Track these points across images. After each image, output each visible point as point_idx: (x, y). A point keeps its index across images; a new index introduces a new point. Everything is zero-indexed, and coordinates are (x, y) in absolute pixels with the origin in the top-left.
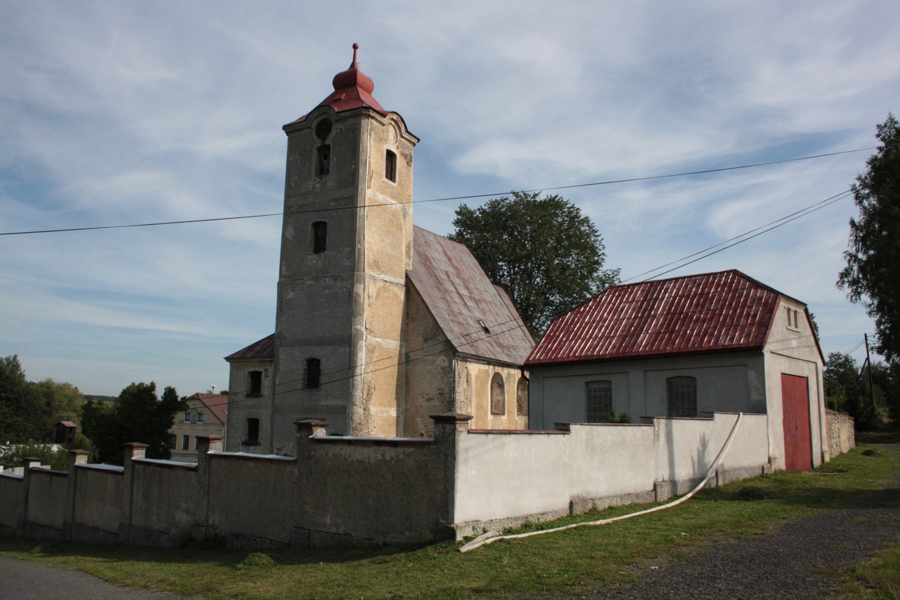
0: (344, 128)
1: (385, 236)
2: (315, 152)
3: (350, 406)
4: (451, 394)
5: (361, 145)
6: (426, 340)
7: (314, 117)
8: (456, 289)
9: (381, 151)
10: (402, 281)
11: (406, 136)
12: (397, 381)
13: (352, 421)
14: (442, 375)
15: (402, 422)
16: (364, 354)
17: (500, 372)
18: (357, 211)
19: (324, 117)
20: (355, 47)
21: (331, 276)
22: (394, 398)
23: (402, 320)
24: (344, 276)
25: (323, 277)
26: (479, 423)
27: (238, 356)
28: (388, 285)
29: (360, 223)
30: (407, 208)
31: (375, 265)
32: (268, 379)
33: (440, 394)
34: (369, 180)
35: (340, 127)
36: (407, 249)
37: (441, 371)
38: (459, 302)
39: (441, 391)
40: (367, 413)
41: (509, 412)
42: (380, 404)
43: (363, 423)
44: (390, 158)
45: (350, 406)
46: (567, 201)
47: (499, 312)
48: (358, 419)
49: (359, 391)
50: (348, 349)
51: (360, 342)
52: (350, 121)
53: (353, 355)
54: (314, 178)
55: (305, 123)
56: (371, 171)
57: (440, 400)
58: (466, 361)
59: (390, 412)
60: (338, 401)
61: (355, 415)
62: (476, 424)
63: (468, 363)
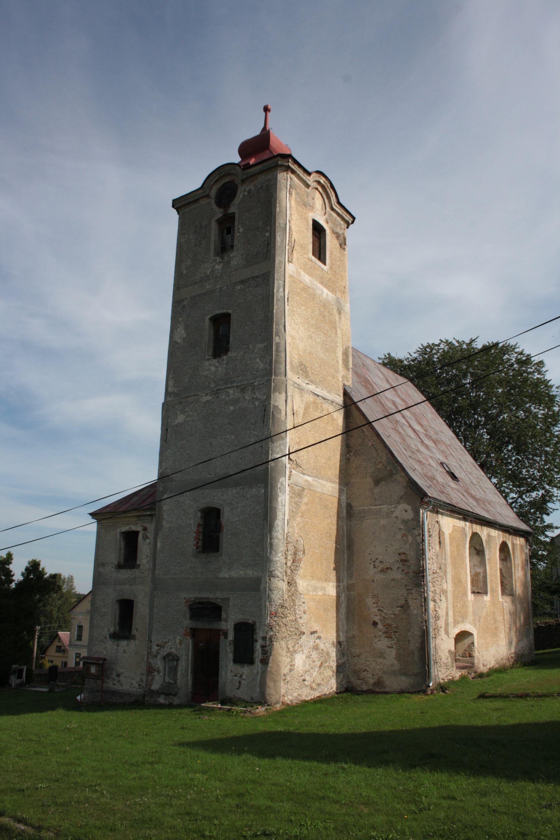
0: (253, 190)
1: (314, 332)
2: (214, 226)
3: (267, 579)
4: (420, 560)
5: (278, 205)
6: (377, 482)
7: (214, 181)
8: (408, 422)
9: (305, 219)
10: (340, 400)
11: (337, 209)
12: (336, 543)
13: (270, 602)
14: (404, 532)
15: (344, 605)
16: (287, 497)
17: (479, 532)
18: (273, 292)
19: (227, 180)
20: (266, 109)
21: (237, 386)
22: (332, 568)
23: (341, 455)
24: (256, 384)
25: (225, 388)
26: (457, 606)
27: (107, 510)
28: (320, 401)
29: (278, 308)
30: (342, 303)
31: (302, 370)
32: (148, 540)
33: (402, 561)
34: (290, 251)
35: (247, 189)
36: (344, 357)
37: (402, 527)
38: (415, 437)
39: (403, 557)
40: (293, 589)
41: (493, 591)
42: (312, 577)
43: (287, 605)
44: (317, 234)
45: (267, 579)
46: (516, 345)
47: (461, 457)
48: (279, 599)
49: (280, 555)
50: (263, 491)
51: (282, 479)
52: (262, 178)
53: (271, 500)
54: (213, 258)
55: (201, 191)
56: (293, 240)
57: (403, 570)
58: (437, 513)
59: (327, 589)
60: (248, 572)
61: (275, 592)
62: (453, 607)
63: (440, 516)
